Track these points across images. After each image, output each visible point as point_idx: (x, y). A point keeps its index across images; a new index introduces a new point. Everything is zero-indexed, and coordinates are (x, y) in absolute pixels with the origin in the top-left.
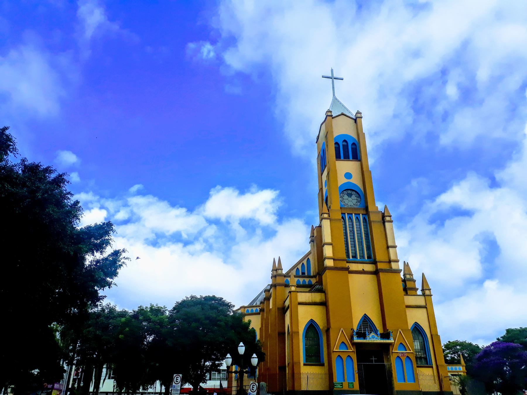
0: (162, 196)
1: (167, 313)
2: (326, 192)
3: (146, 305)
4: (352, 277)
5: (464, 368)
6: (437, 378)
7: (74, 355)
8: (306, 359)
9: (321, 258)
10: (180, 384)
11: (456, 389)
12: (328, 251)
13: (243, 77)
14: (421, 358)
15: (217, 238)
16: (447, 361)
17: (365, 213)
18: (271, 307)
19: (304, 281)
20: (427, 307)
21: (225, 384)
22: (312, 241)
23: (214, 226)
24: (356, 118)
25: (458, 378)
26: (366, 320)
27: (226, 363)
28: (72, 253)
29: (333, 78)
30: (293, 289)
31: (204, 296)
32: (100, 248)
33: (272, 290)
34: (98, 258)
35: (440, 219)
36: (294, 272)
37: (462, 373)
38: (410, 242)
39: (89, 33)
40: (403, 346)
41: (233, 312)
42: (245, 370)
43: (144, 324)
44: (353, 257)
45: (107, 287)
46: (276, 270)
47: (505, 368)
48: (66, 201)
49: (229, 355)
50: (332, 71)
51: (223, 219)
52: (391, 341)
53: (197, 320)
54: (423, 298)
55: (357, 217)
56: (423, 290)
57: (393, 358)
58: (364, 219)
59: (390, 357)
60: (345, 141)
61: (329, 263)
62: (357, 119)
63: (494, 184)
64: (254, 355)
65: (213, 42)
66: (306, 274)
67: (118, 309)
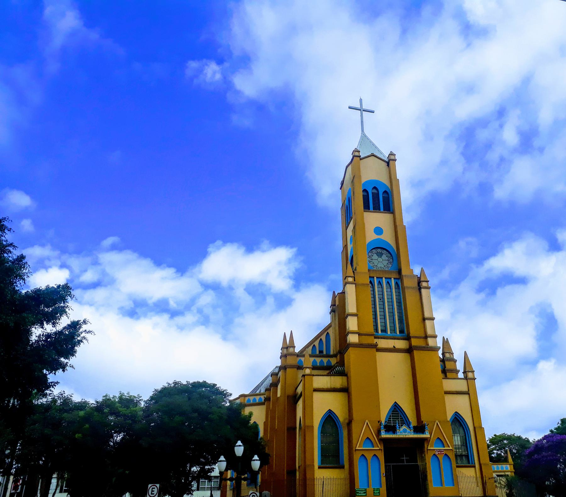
0: (143, 253)
1: (143, 404)
2: (351, 252)
3: (114, 394)
4: (379, 355)
5: (512, 466)
6: (479, 480)
7: (12, 462)
8: (322, 460)
9: (343, 332)
11: (502, 494)
12: (352, 324)
13: (258, 107)
14: (461, 456)
16: (492, 460)
18: (279, 395)
20: (470, 393)
22: (333, 311)
23: (211, 292)
25: (504, 479)
26: (396, 409)
27: (218, 467)
28: (12, 324)
29: (361, 110)
30: (308, 371)
31: (191, 382)
32: (52, 318)
33: (280, 374)
34: (49, 331)
35: (492, 287)
37: (509, 473)
39: (58, 40)
41: (230, 401)
42: (243, 477)
43: (111, 418)
44: (382, 331)
45: (61, 370)
46: (287, 348)
47: (559, 466)
48: (5, 255)
49: (222, 458)
50: (361, 100)
51: (225, 283)
52: (427, 435)
53: (182, 414)
54: (465, 381)
55: (388, 282)
56: (465, 372)
57: (429, 457)
58: (396, 283)
59: (425, 455)
60: (375, 188)
61: (353, 339)
62: (389, 162)
63: (555, 246)
64: (256, 457)
65: (220, 62)
66: (325, 353)
67: (76, 399)
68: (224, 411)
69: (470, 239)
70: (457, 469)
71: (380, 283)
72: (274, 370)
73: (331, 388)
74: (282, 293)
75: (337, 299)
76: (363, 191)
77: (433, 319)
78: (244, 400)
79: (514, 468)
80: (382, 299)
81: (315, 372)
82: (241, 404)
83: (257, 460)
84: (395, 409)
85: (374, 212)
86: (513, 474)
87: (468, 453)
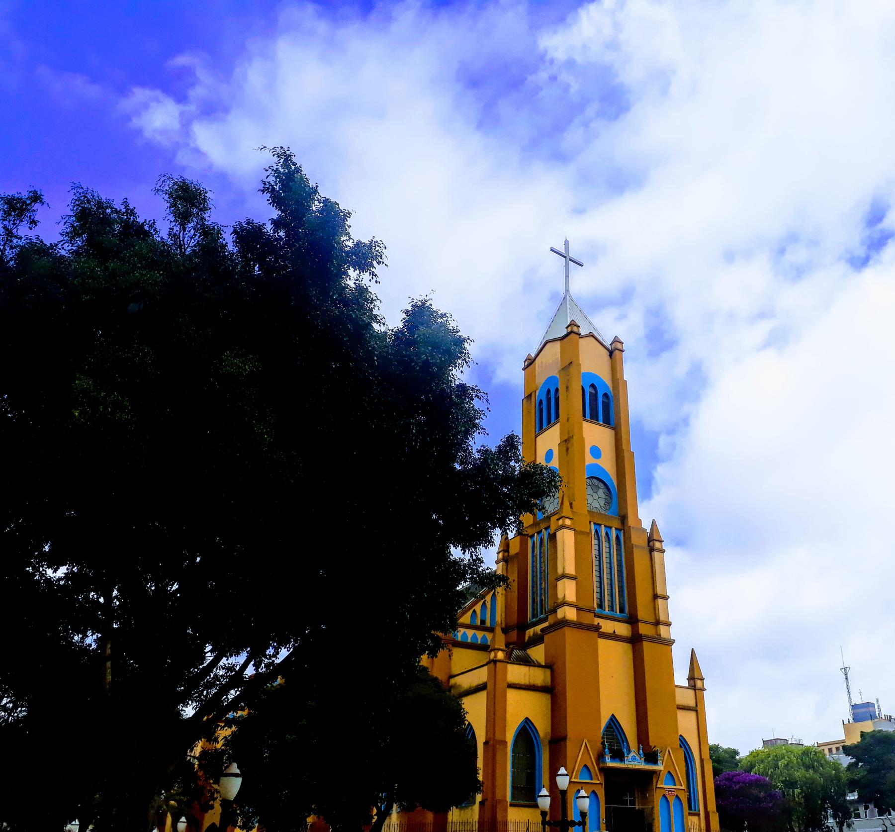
4: (601, 642)
17: (619, 526)
19: (474, 636)
50: (566, 243)
52: (660, 767)
54: (692, 692)
57: (658, 797)
62: (614, 352)
70: (690, 817)
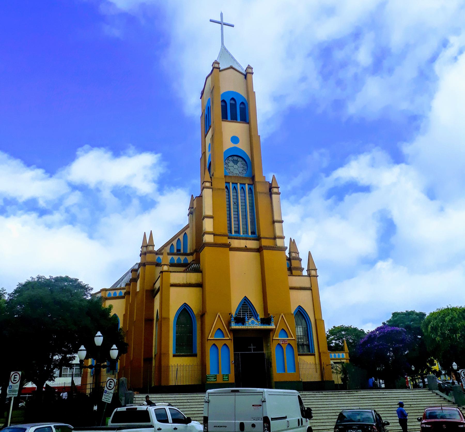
1: (6, 297)
6: (318, 367)
8: (176, 349)
9: (200, 233)
10: (18, 384)
12: (208, 225)
13: (129, 19)
14: (303, 345)
15: (80, 206)
18: (138, 290)
19: (186, 259)
20: (312, 289)
21: (78, 381)
22: (191, 213)
23: (78, 193)
24: (247, 73)
25: (340, 366)
26: (246, 303)
27: (81, 354)
30: (165, 268)
31: (54, 276)
33: (140, 270)
35: (340, 193)
36: (168, 249)
38: (304, 217)
40: (285, 333)
41: (91, 295)
44: (235, 232)
46: (147, 246)
49: (82, 347)
50: (222, 14)
51: (92, 186)
52: (272, 327)
54: (308, 278)
55: (242, 188)
56: (308, 270)
58: (250, 189)
60: (233, 99)
62: (247, 75)
64: (114, 347)
66: (182, 251)
68: (83, 304)
69: (323, 150)
71: (235, 188)
72: (134, 267)
73: (187, 284)
74: (147, 196)
75: (195, 202)
76: (222, 101)
77: (282, 222)
78: (105, 294)
79: (349, 356)
80: (236, 204)
81: (172, 269)
82: (101, 298)
83: (115, 349)
84: (245, 302)
85: (232, 122)
86: (348, 361)
87: (309, 343)
